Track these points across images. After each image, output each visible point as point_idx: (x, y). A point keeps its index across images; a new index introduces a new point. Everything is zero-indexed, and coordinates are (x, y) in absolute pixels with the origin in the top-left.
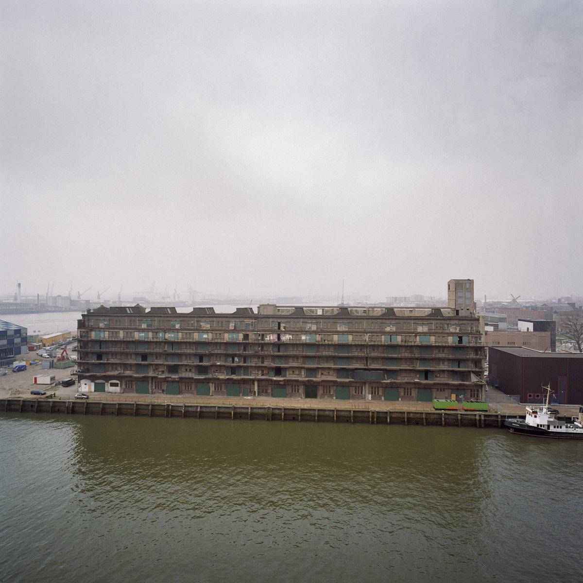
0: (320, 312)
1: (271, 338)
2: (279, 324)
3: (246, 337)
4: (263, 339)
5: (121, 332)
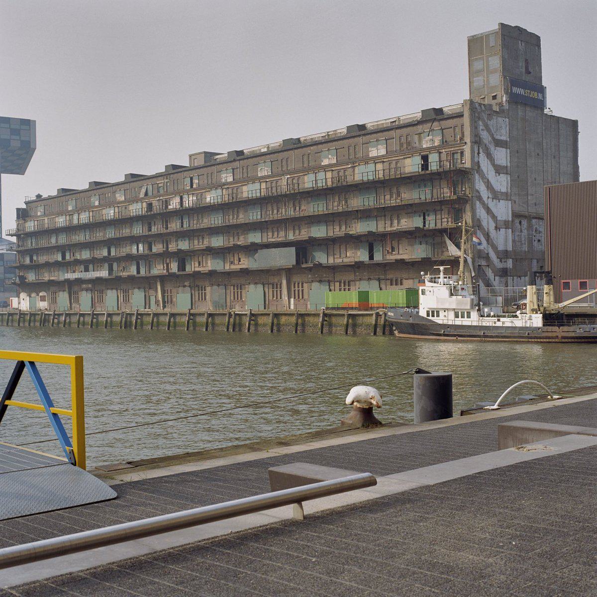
0: (265, 150)
1: (174, 204)
2: (192, 179)
3: (150, 206)
4: (167, 207)
5: (46, 219)
